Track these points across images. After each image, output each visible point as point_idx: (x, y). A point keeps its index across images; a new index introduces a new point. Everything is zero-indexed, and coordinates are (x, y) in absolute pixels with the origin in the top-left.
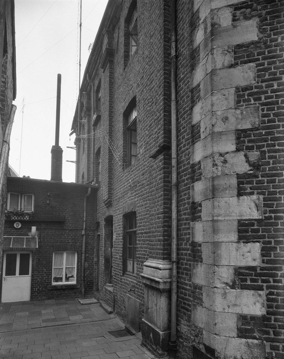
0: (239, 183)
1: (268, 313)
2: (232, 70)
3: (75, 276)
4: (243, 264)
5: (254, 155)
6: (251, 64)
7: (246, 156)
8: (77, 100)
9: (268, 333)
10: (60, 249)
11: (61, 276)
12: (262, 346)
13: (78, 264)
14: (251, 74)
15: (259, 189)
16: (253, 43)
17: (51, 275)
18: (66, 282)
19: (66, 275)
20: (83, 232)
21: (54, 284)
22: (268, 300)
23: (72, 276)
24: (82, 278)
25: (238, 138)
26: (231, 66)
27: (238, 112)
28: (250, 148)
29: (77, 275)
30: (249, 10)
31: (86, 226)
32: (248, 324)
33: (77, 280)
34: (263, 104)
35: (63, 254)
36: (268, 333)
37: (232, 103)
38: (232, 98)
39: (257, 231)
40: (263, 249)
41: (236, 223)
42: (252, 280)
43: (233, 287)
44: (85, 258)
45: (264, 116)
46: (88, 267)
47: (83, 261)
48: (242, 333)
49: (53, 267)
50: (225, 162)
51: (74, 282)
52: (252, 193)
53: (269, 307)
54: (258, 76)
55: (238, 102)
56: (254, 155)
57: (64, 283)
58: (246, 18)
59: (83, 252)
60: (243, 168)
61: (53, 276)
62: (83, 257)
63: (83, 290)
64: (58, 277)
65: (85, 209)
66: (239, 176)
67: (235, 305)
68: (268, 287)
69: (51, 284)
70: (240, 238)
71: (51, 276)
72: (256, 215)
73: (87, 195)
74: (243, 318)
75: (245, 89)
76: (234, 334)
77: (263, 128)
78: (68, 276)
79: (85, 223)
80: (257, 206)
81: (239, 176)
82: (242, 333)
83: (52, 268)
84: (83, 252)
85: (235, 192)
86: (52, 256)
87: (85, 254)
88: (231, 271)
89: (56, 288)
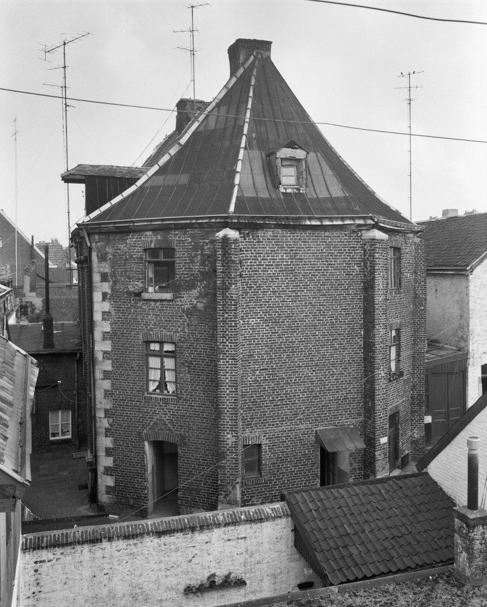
0: (106, 432)
1: (115, 485)
2: (103, 381)
3: (70, 431)
4: (107, 465)
5: (111, 420)
6: (109, 380)
7: (108, 420)
8: (85, 197)
9: (115, 493)
10: (56, 409)
11: (58, 432)
12: (113, 498)
13: (72, 419)
14: (109, 385)
15: (112, 435)
16: (110, 371)
17: (49, 431)
18: (62, 436)
19: (62, 430)
20: (75, 392)
21: (52, 439)
22: (116, 480)
23: (68, 431)
24: (77, 433)
25: (105, 412)
26: (103, 379)
27: (105, 401)
28: (109, 417)
29: (72, 430)
30: (108, 355)
31: (78, 386)
32: (109, 489)
33: (72, 434)
34: (113, 399)
35: (58, 412)
36: (115, 493)
37: (103, 396)
38: (103, 394)
39: (111, 452)
40: (114, 460)
41: (105, 448)
42: (111, 472)
43: (104, 474)
44: (78, 415)
45: (114, 404)
46: (81, 423)
47: (76, 418)
48: (107, 493)
49: (50, 424)
50: (101, 421)
51: (69, 437)
52: (110, 437)
53: (116, 483)
54: (112, 386)
55: (105, 396)
56: (111, 420)
57: (60, 437)
58: (108, 359)
59: (76, 410)
60: (107, 426)
61: (50, 432)
62: (76, 415)
63: (78, 444)
64: (55, 432)
65: (76, 371)
66: (106, 429)
67: (105, 482)
68: (116, 475)
69: (49, 440)
70: (106, 454)
71: (49, 433)
72: (111, 446)
73: (76, 359)
74: (107, 487)
75: (107, 391)
76: (104, 493)
77: (114, 410)
78: (64, 431)
79: (76, 383)
80: (112, 442)
81: (106, 429)
82: (107, 493)
83: (49, 426)
84: (76, 410)
85: (104, 435)
86: (49, 415)
87: (78, 411)
88: (104, 468)
89: (53, 443)
